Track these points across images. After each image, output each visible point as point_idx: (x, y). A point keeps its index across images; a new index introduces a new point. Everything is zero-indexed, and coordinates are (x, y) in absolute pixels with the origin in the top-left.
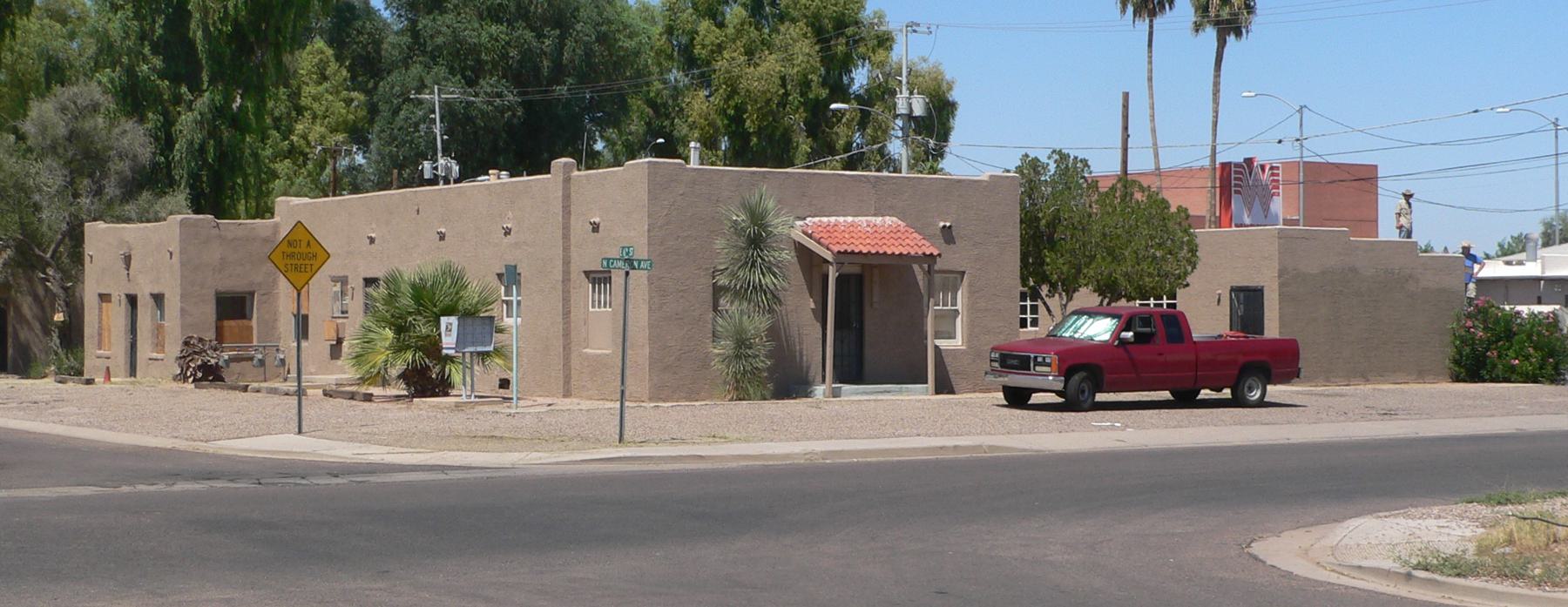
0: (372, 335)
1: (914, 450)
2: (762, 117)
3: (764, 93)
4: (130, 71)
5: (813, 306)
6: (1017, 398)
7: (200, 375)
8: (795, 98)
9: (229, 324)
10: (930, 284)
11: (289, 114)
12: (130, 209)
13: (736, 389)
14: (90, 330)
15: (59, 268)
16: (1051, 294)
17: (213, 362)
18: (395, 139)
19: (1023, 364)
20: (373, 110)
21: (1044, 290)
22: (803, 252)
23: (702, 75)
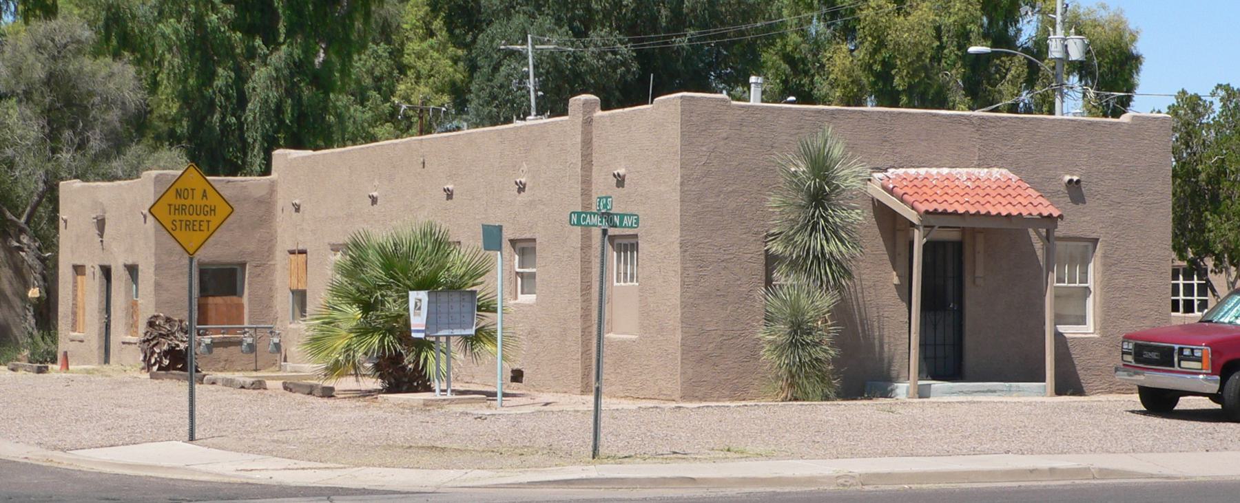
0: (336, 314)
1: (991, 474)
2: (915, 73)
3: (916, 45)
4: (198, 21)
5: (896, 280)
6: (1159, 403)
7: (166, 362)
8: (951, 50)
9: (214, 301)
10: (1049, 252)
11: (390, 74)
12: (117, 165)
13: (791, 385)
14: (64, 307)
15: (36, 236)
16: (1219, 267)
17: (182, 346)
18: (495, 98)
19: (1165, 358)
20: (473, 68)
21: (1209, 263)
22: (883, 214)
23: (846, 24)
